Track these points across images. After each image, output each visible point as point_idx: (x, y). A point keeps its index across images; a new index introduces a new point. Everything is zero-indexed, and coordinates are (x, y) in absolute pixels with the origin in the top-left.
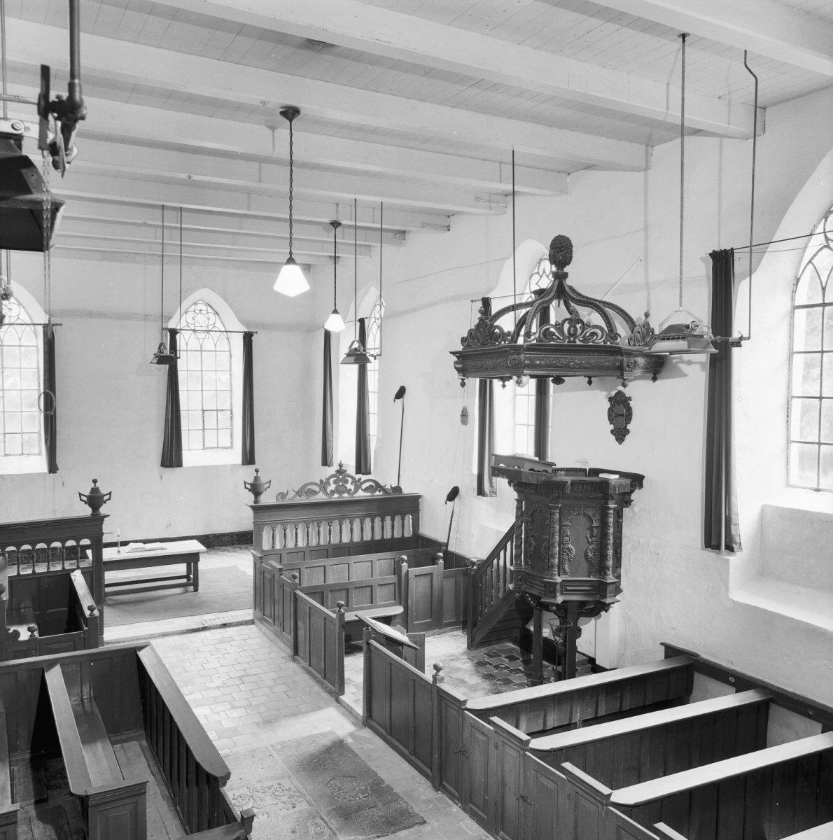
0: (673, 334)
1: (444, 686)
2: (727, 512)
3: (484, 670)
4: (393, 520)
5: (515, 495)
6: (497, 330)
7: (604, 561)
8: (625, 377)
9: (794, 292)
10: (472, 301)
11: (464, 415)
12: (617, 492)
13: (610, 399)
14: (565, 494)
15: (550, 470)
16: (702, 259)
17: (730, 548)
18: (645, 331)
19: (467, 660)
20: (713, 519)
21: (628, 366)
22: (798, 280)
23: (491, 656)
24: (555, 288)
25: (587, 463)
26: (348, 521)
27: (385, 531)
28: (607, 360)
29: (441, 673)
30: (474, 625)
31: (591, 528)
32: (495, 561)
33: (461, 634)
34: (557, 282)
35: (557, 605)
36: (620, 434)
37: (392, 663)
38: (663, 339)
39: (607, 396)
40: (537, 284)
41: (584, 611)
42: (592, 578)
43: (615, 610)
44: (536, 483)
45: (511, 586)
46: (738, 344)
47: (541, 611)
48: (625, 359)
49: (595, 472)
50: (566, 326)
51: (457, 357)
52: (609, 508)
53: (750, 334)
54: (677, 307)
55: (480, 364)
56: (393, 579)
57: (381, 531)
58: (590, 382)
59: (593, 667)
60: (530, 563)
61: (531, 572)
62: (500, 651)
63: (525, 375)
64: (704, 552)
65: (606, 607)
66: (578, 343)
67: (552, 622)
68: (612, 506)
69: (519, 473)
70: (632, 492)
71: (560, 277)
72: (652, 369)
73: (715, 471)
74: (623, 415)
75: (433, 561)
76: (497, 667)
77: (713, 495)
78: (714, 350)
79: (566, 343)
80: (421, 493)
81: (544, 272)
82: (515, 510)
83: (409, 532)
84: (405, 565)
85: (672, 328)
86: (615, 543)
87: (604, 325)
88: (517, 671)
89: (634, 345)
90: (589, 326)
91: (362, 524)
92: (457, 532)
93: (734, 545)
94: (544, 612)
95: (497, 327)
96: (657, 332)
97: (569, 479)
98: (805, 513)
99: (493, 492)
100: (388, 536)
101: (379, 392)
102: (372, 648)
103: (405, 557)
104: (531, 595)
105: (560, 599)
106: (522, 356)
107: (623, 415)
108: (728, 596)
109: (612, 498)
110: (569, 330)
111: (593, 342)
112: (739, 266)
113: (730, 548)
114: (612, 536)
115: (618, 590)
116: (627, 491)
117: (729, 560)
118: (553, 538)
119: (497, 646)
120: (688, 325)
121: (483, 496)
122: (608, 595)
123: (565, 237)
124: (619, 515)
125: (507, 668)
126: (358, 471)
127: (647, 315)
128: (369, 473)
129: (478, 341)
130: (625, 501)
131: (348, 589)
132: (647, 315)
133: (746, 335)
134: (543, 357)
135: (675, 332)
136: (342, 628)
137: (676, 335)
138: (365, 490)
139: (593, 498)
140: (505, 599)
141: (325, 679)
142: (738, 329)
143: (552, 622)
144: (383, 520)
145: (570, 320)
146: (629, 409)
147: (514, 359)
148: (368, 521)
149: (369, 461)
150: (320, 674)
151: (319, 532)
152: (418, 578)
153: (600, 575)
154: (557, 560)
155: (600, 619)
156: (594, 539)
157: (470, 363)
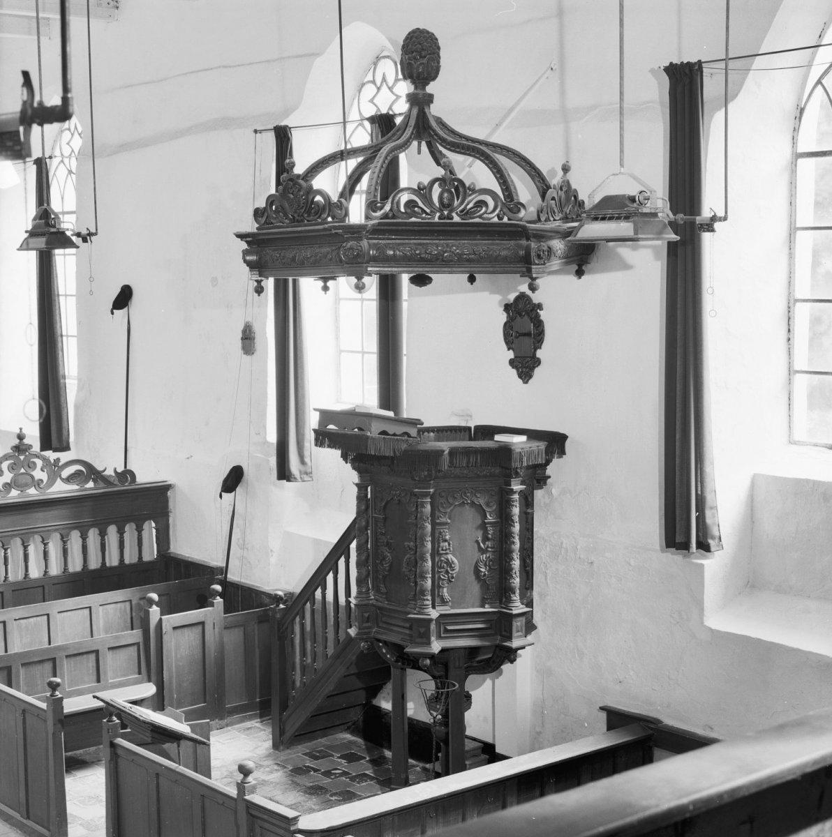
0: (610, 211)
1: (256, 799)
2: (699, 489)
3: (306, 781)
4: (121, 532)
5: (354, 477)
6: (318, 198)
7: (506, 579)
8: (534, 276)
9: (796, 130)
10: (256, 131)
11: (248, 338)
12: (525, 464)
13: (507, 308)
14: (439, 471)
15: (413, 432)
16: (652, 71)
17: (704, 546)
18: (563, 196)
19: (276, 767)
20: (678, 500)
21: (539, 257)
22: (802, 111)
23: (316, 758)
24: (412, 122)
25: (471, 416)
26: (38, 538)
27: (107, 553)
28: (503, 248)
29: (250, 779)
30: (284, 706)
31: (483, 526)
32: (318, 593)
33: (258, 725)
34: (415, 111)
35: (432, 657)
36: (525, 366)
37: (159, 773)
38: (596, 219)
39: (500, 302)
40: (372, 101)
41: (475, 664)
42: (488, 609)
43: (525, 659)
44: (392, 454)
45: (352, 632)
46: (709, 227)
47: (403, 670)
48: (533, 245)
49: (487, 432)
50: (436, 191)
51: (247, 242)
52: (512, 492)
53: (726, 212)
54: (617, 168)
55: (289, 254)
56: (135, 636)
57: (100, 554)
58: (472, 279)
59: (489, 754)
60: (384, 590)
61: (385, 604)
62: (331, 747)
63: (370, 275)
64: (665, 554)
65: (510, 655)
66: (456, 219)
67: (424, 685)
68: (517, 487)
69: (362, 440)
70: (548, 462)
71: (420, 101)
72: (576, 258)
73: (679, 415)
74: (528, 334)
75: (203, 601)
76: (327, 774)
77: (677, 453)
78: (674, 237)
79: (436, 219)
80: (171, 480)
81: (384, 79)
82: (355, 502)
83: (151, 552)
84: (155, 611)
85: (608, 201)
86: (522, 549)
87: (497, 189)
88: (363, 777)
89: (547, 220)
90: (473, 191)
91: (64, 542)
92: (243, 547)
93: (711, 541)
94: (409, 671)
95: (319, 192)
96: (588, 206)
97: (445, 446)
98: (816, 484)
99: (306, 473)
100: (112, 560)
101: (79, 296)
102: (119, 752)
103: (155, 596)
104: (385, 643)
105: (436, 646)
106: (365, 243)
107: (528, 334)
108: (702, 623)
109: (517, 474)
110: (441, 198)
111: (480, 217)
112: (711, 86)
113: (704, 546)
114: (517, 538)
115: (530, 627)
116: (540, 461)
117: (702, 565)
118: (423, 545)
119: (323, 741)
120: (634, 197)
121: (289, 480)
122: (515, 634)
123: (428, 32)
124: (527, 501)
125: (345, 774)
126: (46, 443)
127: (566, 169)
128: (66, 448)
129: (286, 215)
130: (537, 477)
131: (54, 660)
132: (566, 169)
133: (721, 214)
134: (399, 244)
135: (614, 208)
136: (60, 726)
137: (615, 212)
138: (69, 480)
139: (485, 476)
140: (337, 656)
141: (28, 818)
142: (711, 203)
143: (424, 685)
144: (103, 534)
145: (442, 181)
146: (539, 324)
147: (351, 248)
148: (75, 537)
149: (65, 424)
150: (19, 812)
151: (46, 554)
152: (179, 631)
153: (501, 602)
154: (429, 583)
155: (501, 678)
156: (489, 543)
157: (271, 253)
